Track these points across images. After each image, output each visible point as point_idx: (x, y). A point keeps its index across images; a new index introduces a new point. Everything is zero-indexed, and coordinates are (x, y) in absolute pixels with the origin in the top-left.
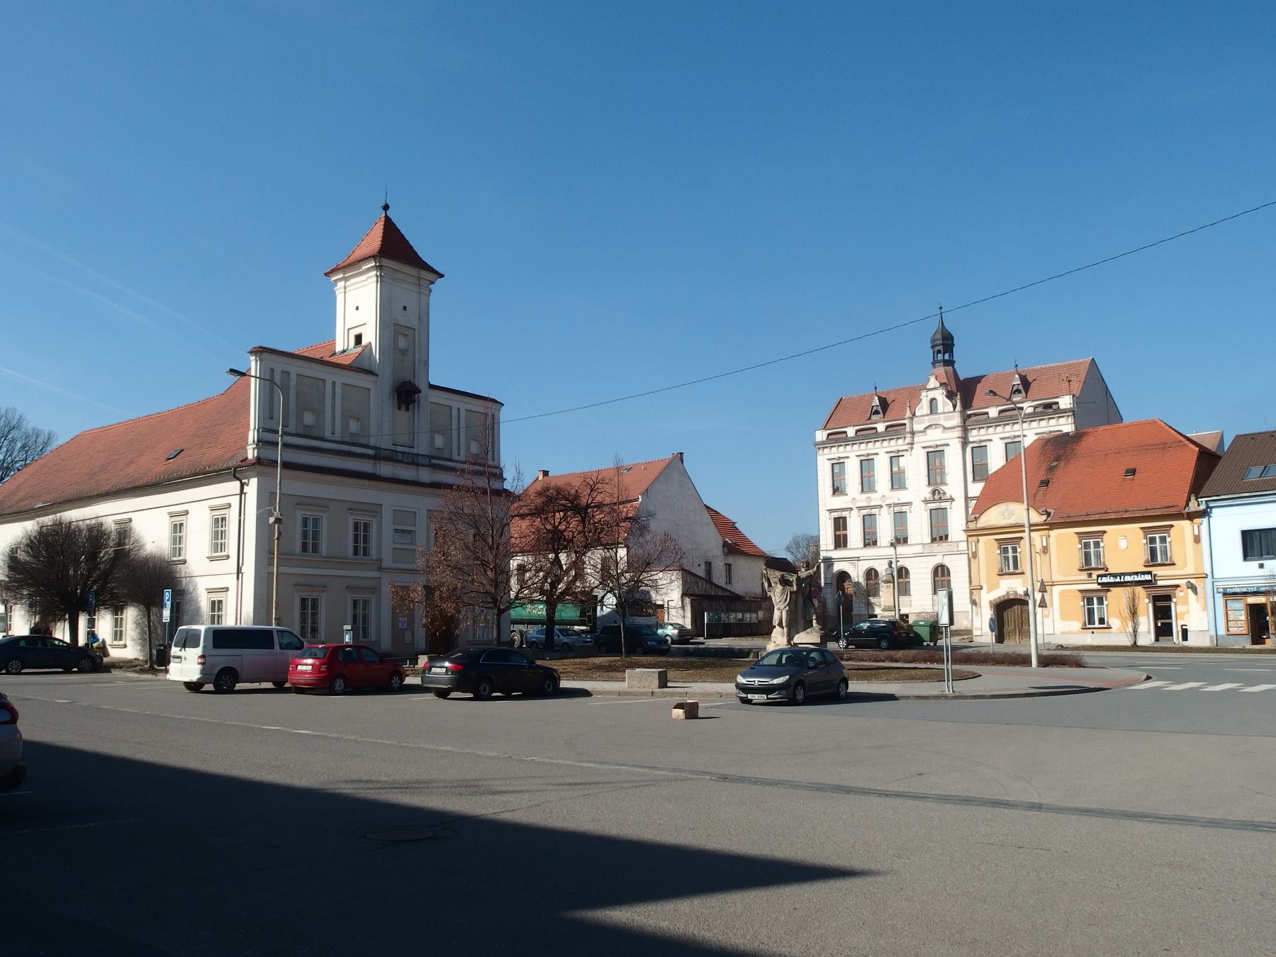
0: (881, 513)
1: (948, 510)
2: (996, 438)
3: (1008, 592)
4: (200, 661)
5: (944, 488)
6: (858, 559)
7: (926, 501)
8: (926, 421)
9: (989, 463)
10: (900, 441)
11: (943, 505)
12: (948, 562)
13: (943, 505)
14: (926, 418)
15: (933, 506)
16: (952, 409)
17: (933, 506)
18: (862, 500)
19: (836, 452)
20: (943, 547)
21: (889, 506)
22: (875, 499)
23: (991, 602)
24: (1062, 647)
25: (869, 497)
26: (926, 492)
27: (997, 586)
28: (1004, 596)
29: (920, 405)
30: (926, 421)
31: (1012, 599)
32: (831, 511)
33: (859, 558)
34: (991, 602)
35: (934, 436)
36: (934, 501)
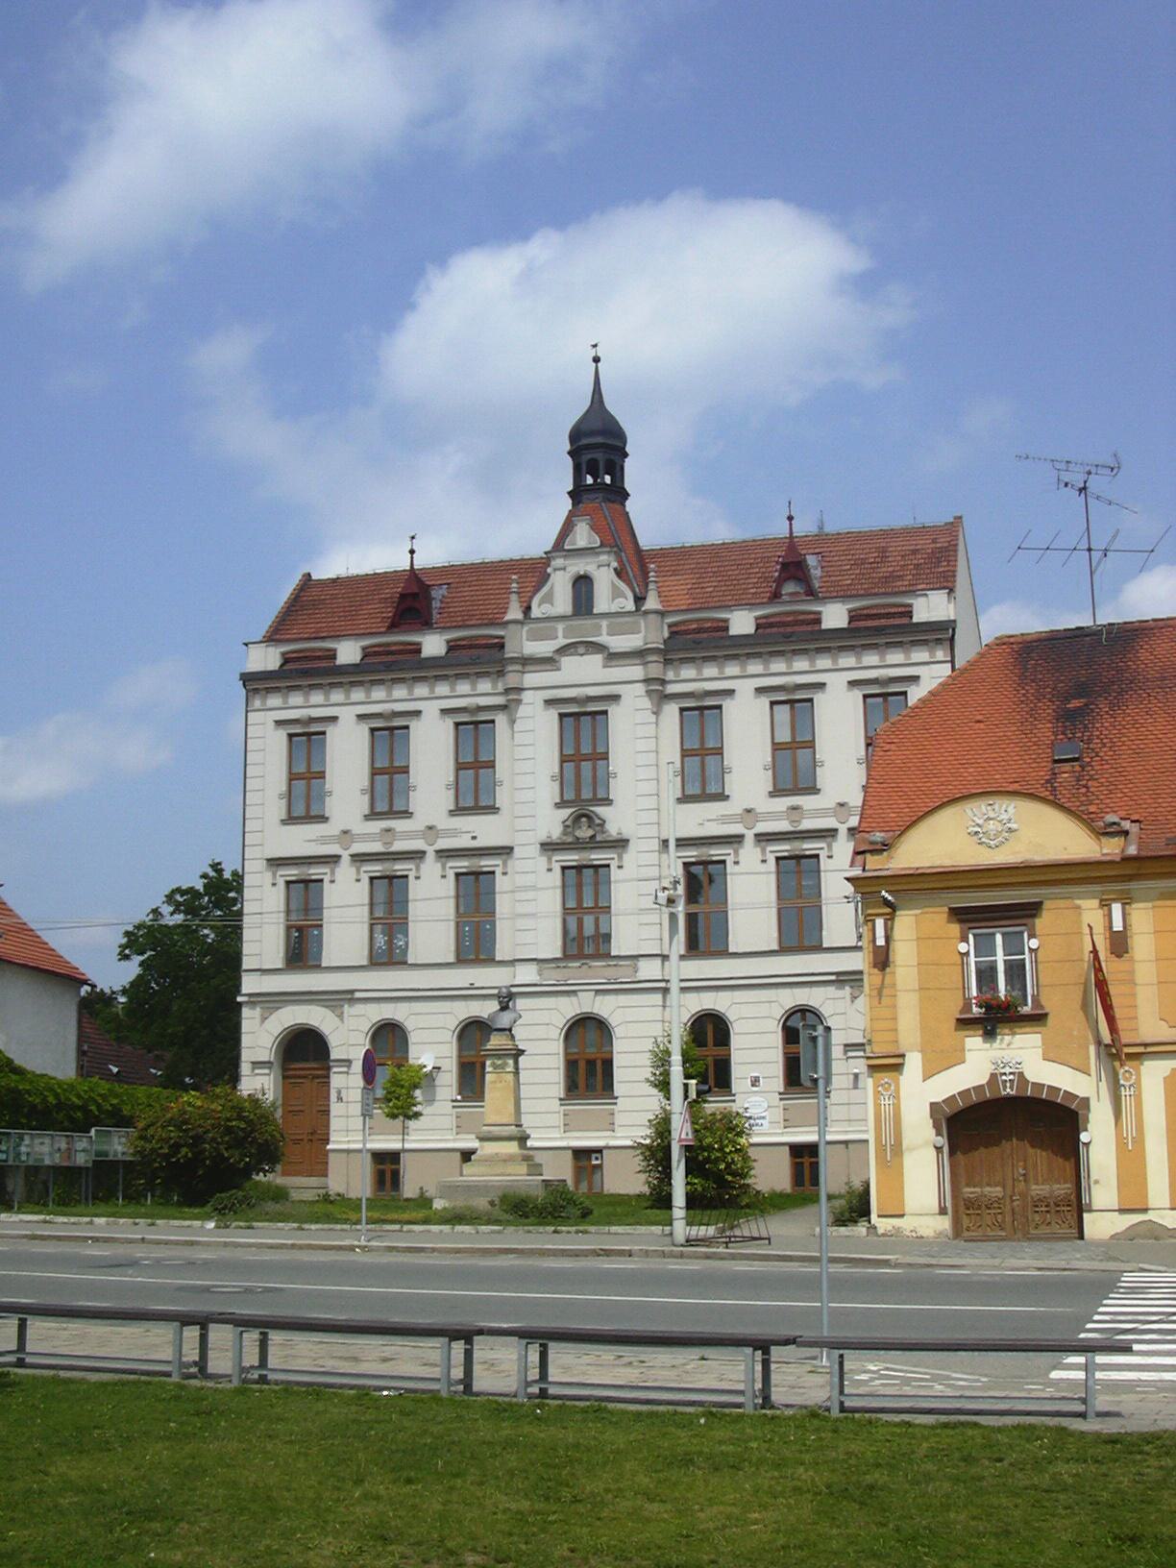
0: (741, 859)
1: (326, 884)
2: (431, 709)
3: (993, 1076)
4: (754, 1164)
5: (600, 810)
6: (348, 997)
7: (549, 847)
8: (560, 634)
9: (327, 770)
10: (484, 686)
11: (597, 857)
12: (604, 1007)
13: (597, 857)
14: (560, 627)
15: (572, 858)
16: (630, 606)
17: (572, 858)
18: (775, 813)
19: (383, 699)
20: (598, 972)
21: (445, 854)
22: (406, 834)
23: (934, 1107)
24: (539, 1254)
25: (388, 830)
26: (551, 822)
27: (957, 1058)
28: (979, 1089)
29: (545, 589)
30: (560, 634)
31: (1009, 1099)
32: (275, 863)
33: (352, 992)
34: (934, 1107)
35: (583, 673)
36: (577, 845)
